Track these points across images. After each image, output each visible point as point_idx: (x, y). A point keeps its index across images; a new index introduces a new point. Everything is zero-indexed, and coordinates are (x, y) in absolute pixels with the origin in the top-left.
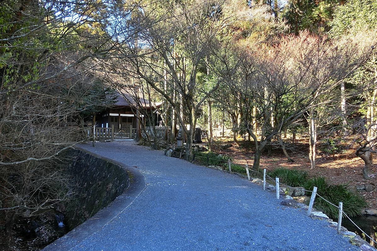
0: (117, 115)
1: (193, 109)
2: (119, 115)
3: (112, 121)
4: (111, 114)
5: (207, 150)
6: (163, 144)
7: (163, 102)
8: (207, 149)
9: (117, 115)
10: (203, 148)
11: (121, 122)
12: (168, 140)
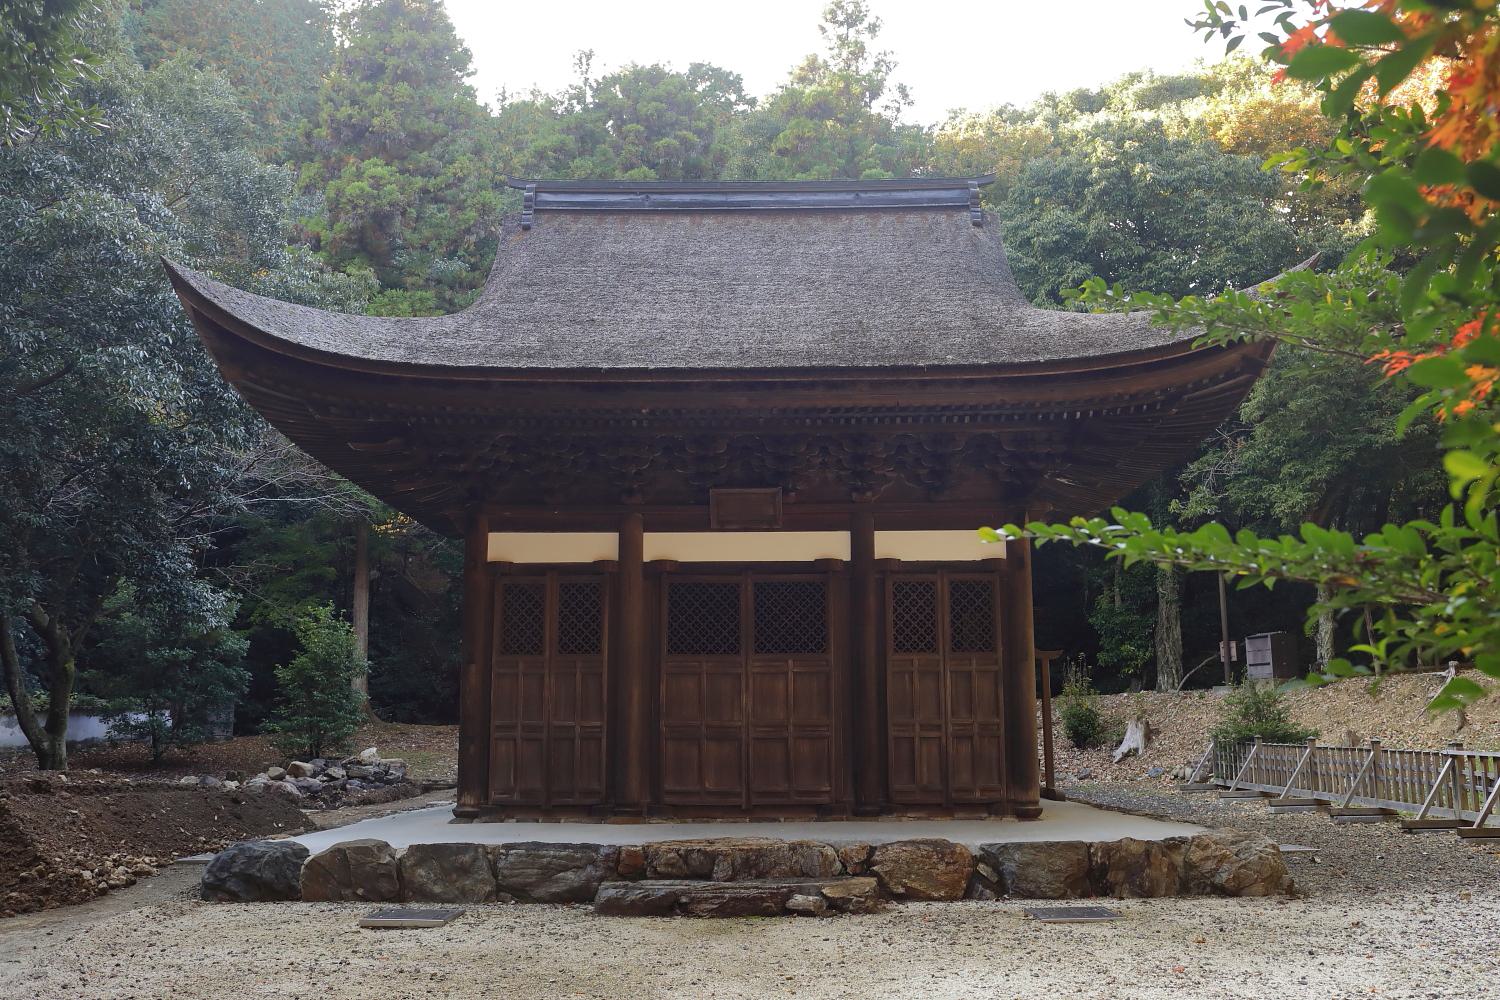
0: (595, 546)
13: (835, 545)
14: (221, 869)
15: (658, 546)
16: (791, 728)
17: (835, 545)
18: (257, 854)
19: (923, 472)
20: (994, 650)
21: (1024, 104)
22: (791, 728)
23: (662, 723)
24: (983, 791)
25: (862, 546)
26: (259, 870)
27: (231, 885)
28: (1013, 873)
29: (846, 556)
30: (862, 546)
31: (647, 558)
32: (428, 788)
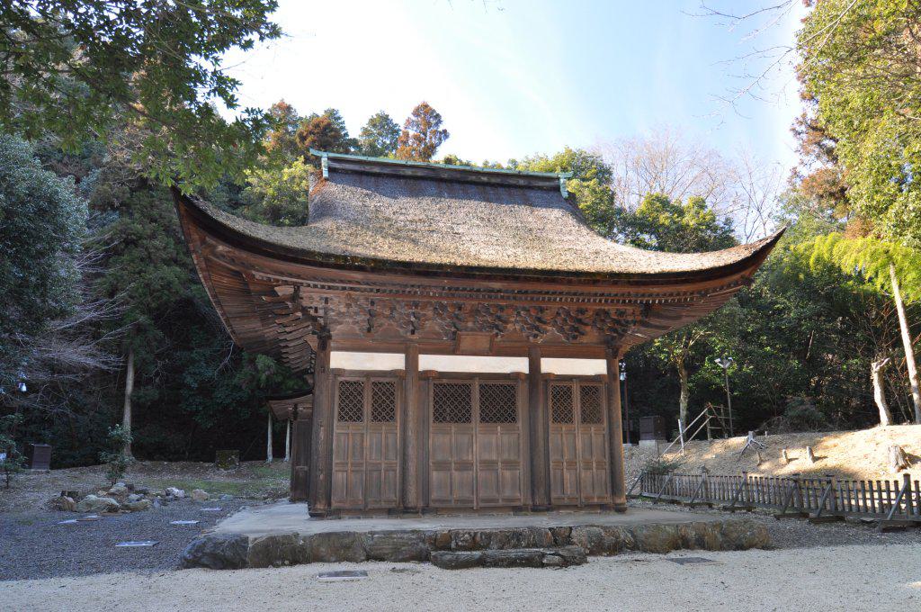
3: (351, 411)
13: (520, 365)
14: (197, 551)
15: (427, 362)
16: (500, 464)
17: (520, 365)
18: (220, 541)
19: (566, 327)
20: (602, 423)
21: (321, 113)
22: (500, 464)
23: (430, 460)
24: (598, 498)
25: (534, 366)
26: (223, 551)
27: (204, 560)
28: (643, 541)
29: (526, 371)
30: (534, 366)
31: (421, 369)
32: (533, 494)
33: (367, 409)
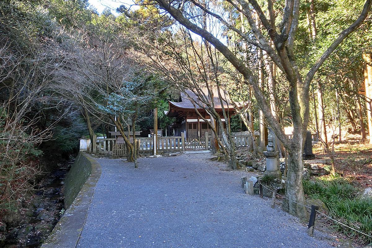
0: (196, 120)
1: (298, 85)
2: (198, 120)
3: (190, 128)
4: (188, 120)
5: (327, 173)
6: (247, 157)
7: (219, 74)
8: (328, 170)
9: (196, 120)
10: (320, 169)
11: (200, 128)
12: (254, 152)
33: (208, 128)
